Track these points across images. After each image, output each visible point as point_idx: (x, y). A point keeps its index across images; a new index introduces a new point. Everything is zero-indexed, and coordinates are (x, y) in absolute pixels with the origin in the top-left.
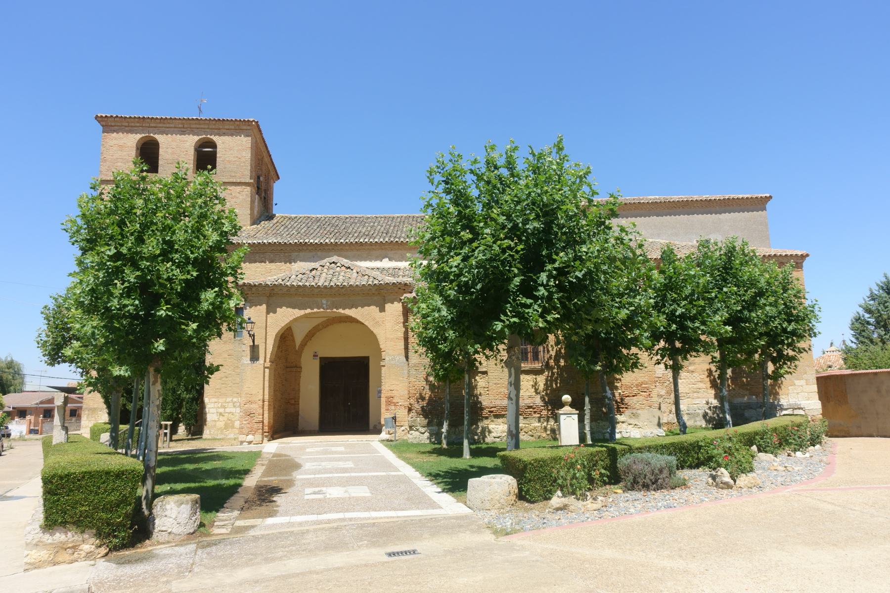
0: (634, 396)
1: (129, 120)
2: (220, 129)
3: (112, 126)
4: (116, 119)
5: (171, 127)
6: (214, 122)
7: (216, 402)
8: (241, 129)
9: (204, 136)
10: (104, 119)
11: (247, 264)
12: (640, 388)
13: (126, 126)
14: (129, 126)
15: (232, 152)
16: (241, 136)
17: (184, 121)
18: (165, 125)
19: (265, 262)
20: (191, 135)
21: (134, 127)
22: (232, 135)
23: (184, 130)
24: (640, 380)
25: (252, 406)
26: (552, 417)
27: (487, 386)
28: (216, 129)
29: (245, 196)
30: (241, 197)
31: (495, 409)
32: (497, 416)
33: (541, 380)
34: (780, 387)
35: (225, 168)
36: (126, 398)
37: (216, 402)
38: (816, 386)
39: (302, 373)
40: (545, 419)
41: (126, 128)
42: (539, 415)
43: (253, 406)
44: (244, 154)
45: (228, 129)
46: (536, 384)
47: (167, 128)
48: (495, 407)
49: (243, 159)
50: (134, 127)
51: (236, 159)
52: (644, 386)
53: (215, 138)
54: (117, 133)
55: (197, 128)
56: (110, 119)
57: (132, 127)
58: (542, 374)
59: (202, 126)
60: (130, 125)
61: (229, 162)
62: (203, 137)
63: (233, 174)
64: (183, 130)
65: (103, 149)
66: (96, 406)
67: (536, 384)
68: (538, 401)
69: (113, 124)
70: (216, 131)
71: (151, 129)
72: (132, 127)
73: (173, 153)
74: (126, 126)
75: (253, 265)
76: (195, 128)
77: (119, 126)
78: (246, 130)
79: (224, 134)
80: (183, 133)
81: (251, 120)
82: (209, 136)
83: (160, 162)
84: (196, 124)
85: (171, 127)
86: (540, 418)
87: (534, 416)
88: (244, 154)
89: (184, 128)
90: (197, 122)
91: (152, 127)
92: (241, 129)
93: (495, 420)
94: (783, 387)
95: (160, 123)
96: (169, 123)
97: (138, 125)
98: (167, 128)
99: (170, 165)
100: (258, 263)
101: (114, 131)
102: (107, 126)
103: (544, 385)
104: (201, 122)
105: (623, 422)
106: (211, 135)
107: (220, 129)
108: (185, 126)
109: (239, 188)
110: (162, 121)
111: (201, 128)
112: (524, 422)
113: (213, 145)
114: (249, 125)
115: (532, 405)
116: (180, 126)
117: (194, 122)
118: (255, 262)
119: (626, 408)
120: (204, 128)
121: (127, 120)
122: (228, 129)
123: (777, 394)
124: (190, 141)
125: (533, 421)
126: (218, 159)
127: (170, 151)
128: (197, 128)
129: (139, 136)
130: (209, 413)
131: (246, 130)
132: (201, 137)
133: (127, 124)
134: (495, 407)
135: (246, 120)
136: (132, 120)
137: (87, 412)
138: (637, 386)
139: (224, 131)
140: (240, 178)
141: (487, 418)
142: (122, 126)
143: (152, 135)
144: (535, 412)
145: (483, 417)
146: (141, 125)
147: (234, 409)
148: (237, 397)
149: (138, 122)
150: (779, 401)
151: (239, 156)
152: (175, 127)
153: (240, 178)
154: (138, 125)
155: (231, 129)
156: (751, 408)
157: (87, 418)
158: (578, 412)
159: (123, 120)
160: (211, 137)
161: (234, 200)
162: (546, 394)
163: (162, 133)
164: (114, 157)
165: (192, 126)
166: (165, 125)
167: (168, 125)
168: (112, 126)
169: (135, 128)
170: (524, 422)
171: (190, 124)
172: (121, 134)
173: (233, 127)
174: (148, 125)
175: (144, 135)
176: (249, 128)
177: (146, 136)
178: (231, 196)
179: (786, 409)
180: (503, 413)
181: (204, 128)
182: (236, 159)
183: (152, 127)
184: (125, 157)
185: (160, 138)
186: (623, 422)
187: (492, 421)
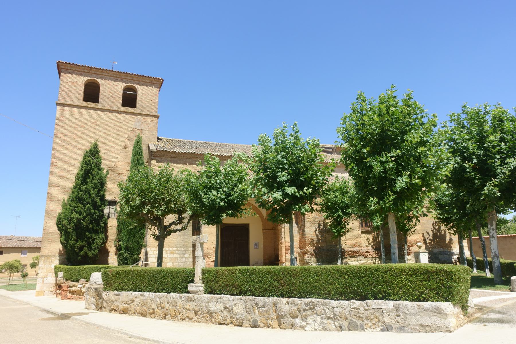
0: (413, 246)
1: (81, 67)
2: (139, 81)
3: (68, 69)
4: (72, 65)
5: (108, 76)
6: (137, 76)
7: (155, 251)
8: (153, 83)
9: (129, 84)
10: (63, 64)
11: (175, 164)
12: (416, 242)
13: (77, 71)
14: (80, 71)
15: (147, 96)
16: (152, 87)
17: (118, 73)
18: (105, 74)
19: (186, 164)
20: (121, 83)
21: (83, 72)
22: (147, 86)
23: (117, 78)
24: (416, 238)
25: (209, 251)
26: (378, 257)
27: (345, 240)
28: (137, 81)
29: (154, 123)
30: (152, 124)
31: (351, 253)
32: (351, 257)
33: (371, 237)
34: (452, 244)
35: (142, 105)
36: (87, 248)
37: (155, 251)
38: (467, 243)
39: (262, 229)
40: (375, 258)
41: (78, 72)
42: (371, 256)
43: (210, 251)
44: (154, 98)
45: (145, 82)
46: (368, 238)
47: (106, 76)
48: (350, 252)
49: (153, 101)
50: (83, 72)
51: (150, 101)
52: (417, 241)
53: (136, 86)
54: (72, 74)
55: (126, 79)
56: (68, 65)
57: (82, 72)
58: (371, 234)
59: (129, 78)
60: (81, 70)
61: (145, 102)
62: (128, 84)
63: (147, 110)
64: (116, 78)
65: (61, 83)
66: (50, 254)
67: (368, 238)
68: (370, 248)
69: (69, 68)
70: (137, 82)
71: (95, 75)
72: (82, 72)
73: (109, 92)
74: (77, 71)
75: (179, 165)
76: (124, 78)
77: (73, 70)
78: (156, 84)
79: (142, 85)
80: (116, 80)
81: (160, 78)
82: (132, 84)
83: (100, 97)
84: (125, 76)
85: (108, 76)
86: (372, 257)
87: (369, 256)
88: (154, 98)
89: (117, 77)
90: (126, 75)
91: (95, 74)
92: (153, 83)
93: (350, 259)
94: (453, 244)
95: (101, 72)
96: (107, 73)
97: (86, 71)
98: (106, 76)
99: (106, 99)
100: (182, 165)
101: (69, 73)
102: (65, 69)
103: (372, 239)
104: (129, 75)
105: (410, 260)
106: (134, 84)
107: (139, 81)
108: (118, 76)
109: (151, 119)
110: (103, 71)
111: (128, 79)
112: (365, 260)
113: (134, 90)
114: (158, 81)
115: (368, 250)
116: (115, 76)
117: (124, 75)
118: (180, 164)
119: (411, 252)
120: (130, 79)
121: (79, 67)
122: (145, 82)
123: (451, 247)
124: (120, 86)
125: (369, 259)
126: (138, 100)
127: (107, 90)
128: (126, 79)
129: (86, 78)
130: (150, 257)
131: (156, 84)
132: (127, 84)
133: (79, 70)
134: (350, 252)
135: (158, 78)
136: (83, 68)
137: (43, 258)
138: (415, 241)
139: (142, 83)
140: (152, 112)
141: (346, 258)
142: (75, 70)
143: (95, 79)
144: (370, 255)
145: (345, 257)
146: (89, 71)
147: (167, 255)
148: (168, 247)
149: (87, 69)
150: (452, 251)
151: (151, 99)
152: (110, 76)
153: (152, 112)
154: (86, 71)
155: (147, 82)
156: (441, 254)
157: (44, 262)
158: (428, 252)
159: (77, 67)
160: (134, 85)
161: (148, 125)
162: (374, 244)
163: (102, 78)
164: (69, 90)
165: (122, 77)
166: (105, 74)
167: (106, 74)
168: (68, 69)
169: (84, 73)
170: (365, 260)
171: (121, 75)
172: (74, 75)
173: (148, 81)
174: (93, 72)
175: (90, 78)
176: (158, 83)
177: (91, 79)
178: (145, 123)
179: (456, 255)
180: (354, 255)
181: (130, 79)
182: (150, 101)
183: (95, 74)
184: (76, 91)
185: (101, 82)
186: (410, 260)
187: (349, 259)
